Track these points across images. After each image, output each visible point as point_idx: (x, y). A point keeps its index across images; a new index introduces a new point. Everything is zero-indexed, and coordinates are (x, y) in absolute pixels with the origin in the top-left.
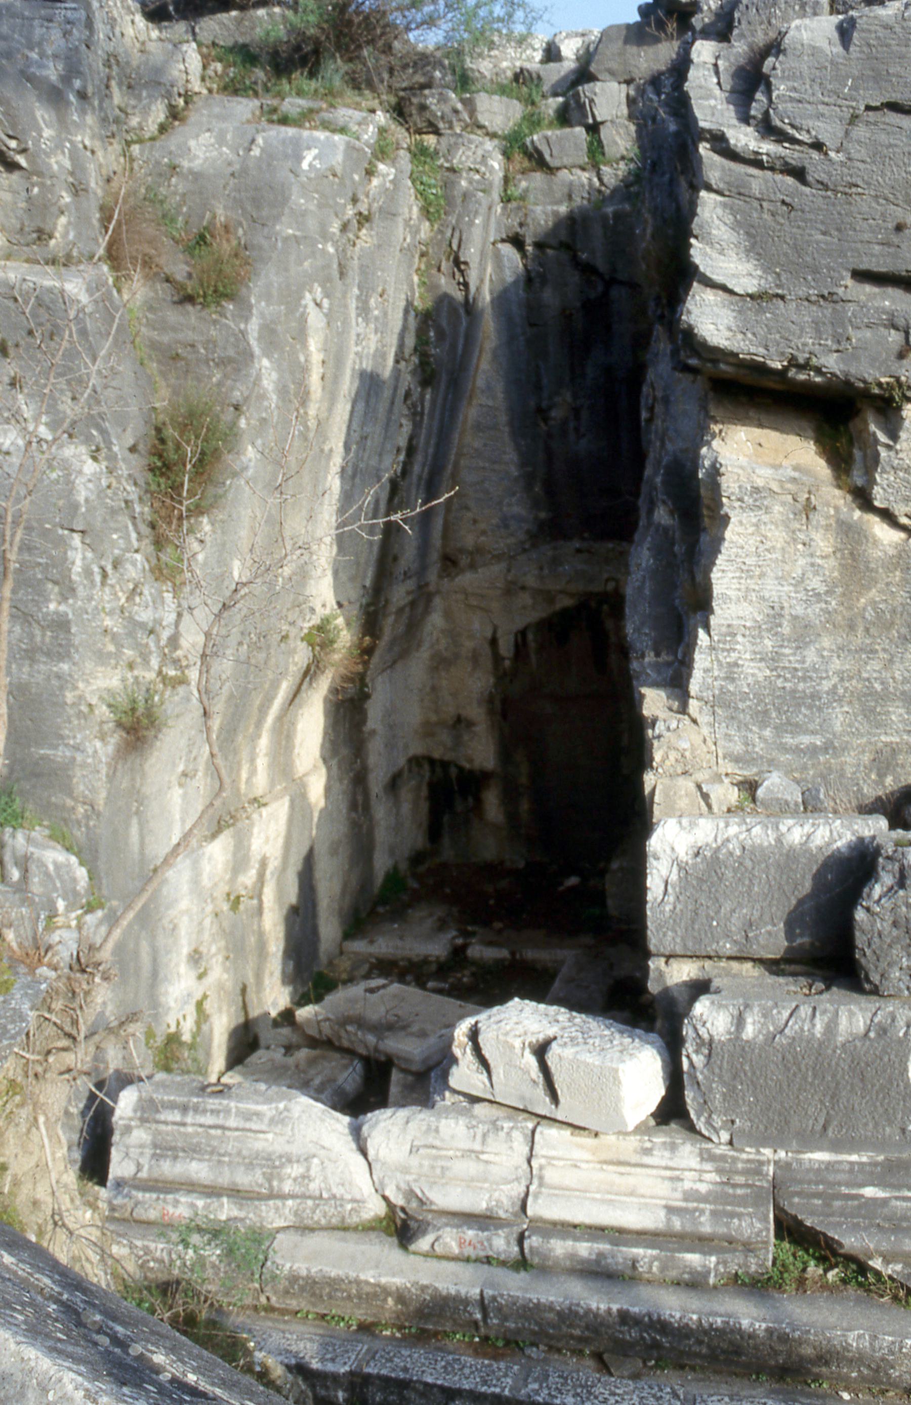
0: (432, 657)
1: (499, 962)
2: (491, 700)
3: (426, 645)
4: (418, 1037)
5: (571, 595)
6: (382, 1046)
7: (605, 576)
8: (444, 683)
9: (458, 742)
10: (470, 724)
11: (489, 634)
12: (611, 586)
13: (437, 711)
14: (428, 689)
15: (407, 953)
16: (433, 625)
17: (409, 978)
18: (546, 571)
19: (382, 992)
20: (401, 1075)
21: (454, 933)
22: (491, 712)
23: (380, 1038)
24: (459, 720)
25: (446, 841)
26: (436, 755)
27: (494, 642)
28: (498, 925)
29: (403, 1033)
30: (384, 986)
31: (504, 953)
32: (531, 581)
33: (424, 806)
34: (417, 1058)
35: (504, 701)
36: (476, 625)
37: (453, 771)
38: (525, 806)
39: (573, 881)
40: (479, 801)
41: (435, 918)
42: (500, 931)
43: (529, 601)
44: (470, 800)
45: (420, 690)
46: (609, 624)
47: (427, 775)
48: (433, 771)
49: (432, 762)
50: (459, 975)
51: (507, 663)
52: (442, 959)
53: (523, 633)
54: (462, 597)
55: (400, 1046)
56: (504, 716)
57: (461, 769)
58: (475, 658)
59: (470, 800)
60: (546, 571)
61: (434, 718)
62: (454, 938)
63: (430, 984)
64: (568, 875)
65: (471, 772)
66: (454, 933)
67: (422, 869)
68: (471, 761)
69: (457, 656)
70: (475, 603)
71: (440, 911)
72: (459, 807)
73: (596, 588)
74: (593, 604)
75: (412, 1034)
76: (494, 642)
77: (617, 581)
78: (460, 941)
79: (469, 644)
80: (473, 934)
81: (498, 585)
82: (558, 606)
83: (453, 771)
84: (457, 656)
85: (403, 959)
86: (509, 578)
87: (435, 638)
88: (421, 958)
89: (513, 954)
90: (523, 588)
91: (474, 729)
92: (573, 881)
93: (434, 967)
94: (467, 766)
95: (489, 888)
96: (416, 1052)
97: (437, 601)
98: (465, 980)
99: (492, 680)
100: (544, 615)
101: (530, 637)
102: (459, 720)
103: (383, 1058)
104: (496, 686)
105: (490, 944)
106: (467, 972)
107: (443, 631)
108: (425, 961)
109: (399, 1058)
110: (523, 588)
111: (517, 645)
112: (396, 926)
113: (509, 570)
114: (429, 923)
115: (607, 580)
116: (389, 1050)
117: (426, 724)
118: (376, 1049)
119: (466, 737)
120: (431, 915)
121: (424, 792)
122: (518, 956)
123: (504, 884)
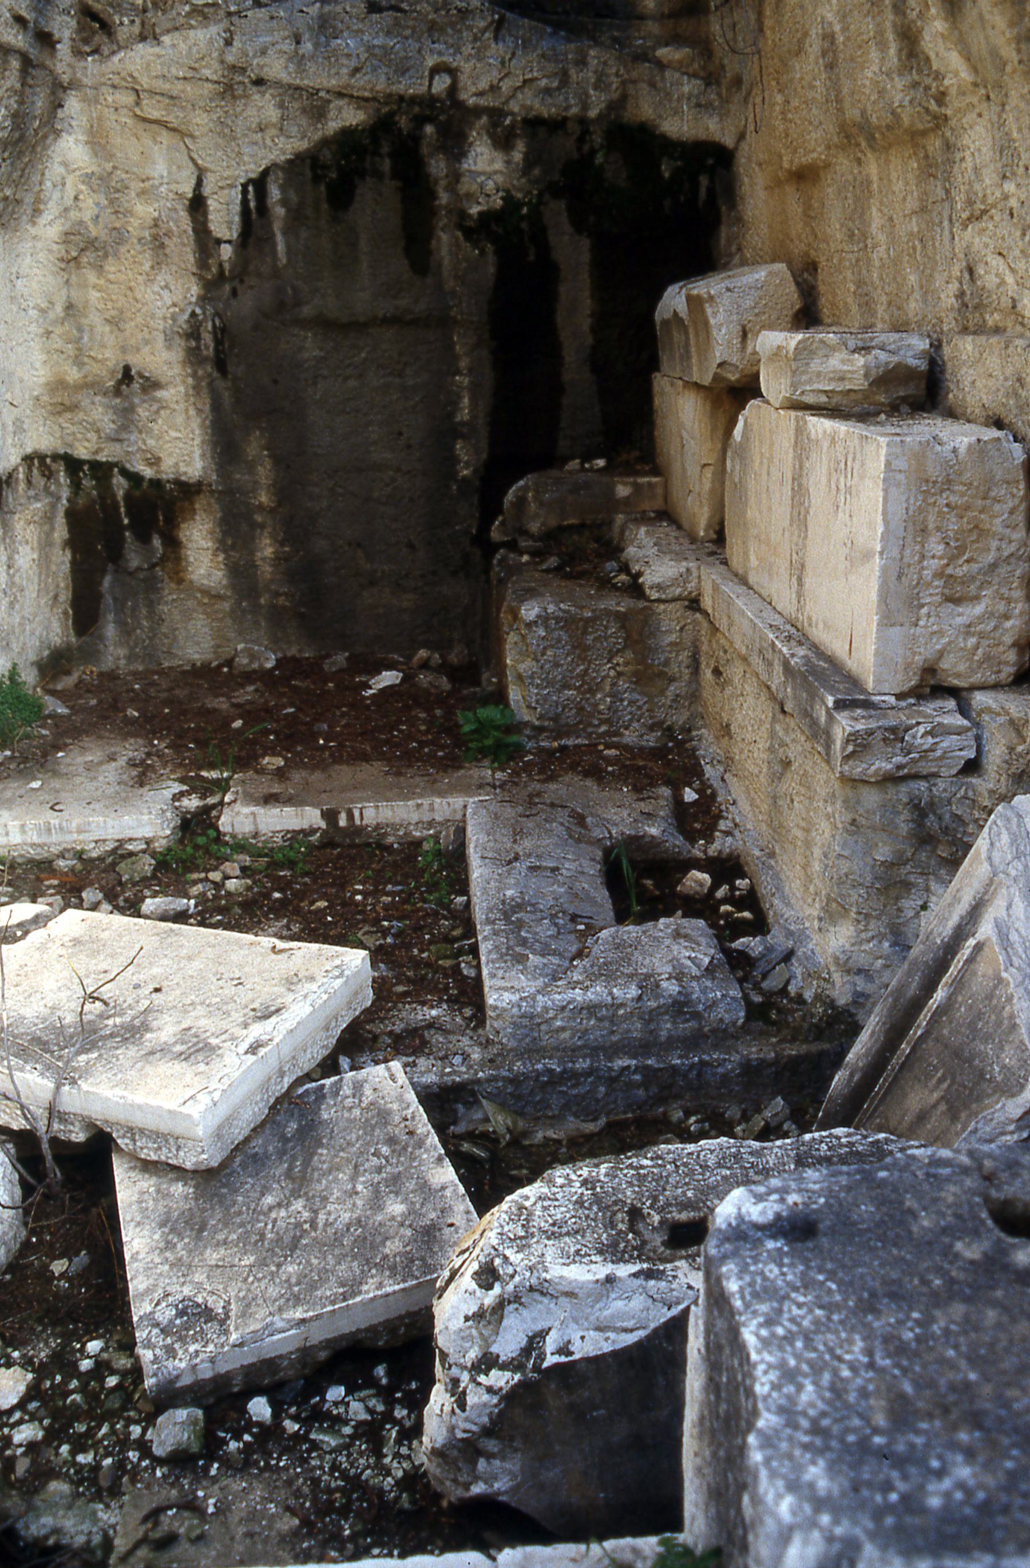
0: (67, 237)
1: (295, 836)
2: (193, 333)
3: (51, 212)
4: (185, 1057)
5: (360, 101)
6: (71, 1100)
7: (430, 62)
8: (94, 295)
9: (126, 417)
10: (151, 385)
11: (188, 190)
12: (441, 84)
13: (78, 361)
14: (59, 309)
15: (71, 839)
16: (65, 164)
17: (89, 895)
18: (308, 47)
19: (36, 936)
20: (148, 1183)
21: (177, 787)
22: (194, 357)
23: (66, 1077)
24: (127, 375)
25: (110, 631)
26: (82, 452)
27: (197, 204)
28: (273, 762)
29: (127, 1054)
30: (39, 921)
31: (311, 817)
32: (277, 68)
33: (62, 560)
34: (200, 1132)
35: (221, 335)
36: (160, 168)
37: (120, 484)
38: (266, 549)
39: (389, 678)
40: (173, 544)
41: (122, 761)
42: (280, 774)
43: (273, 114)
44: (157, 542)
45: (43, 311)
46: (437, 166)
47: (65, 493)
48: (76, 486)
49: (73, 465)
50: (215, 876)
51: (226, 252)
52: (159, 845)
53: (259, 184)
54: (129, 99)
55: (138, 1097)
56: (221, 364)
57: (134, 478)
58: (158, 243)
59: (157, 542)
60: (308, 47)
61: (73, 375)
62: (177, 797)
63: (150, 905)
64: (376, 669)
65: (156, 484)
66: (177, 787)
67: (66, 682)
68: (155, 461)
69: (119, 236)
70: (155, 114)
71: (132, 749)
72: (134, 560)
73: (412, 86)
74: (403, 122)
75: (162, 1051)
76: (197, 204)
77: (452, 72)
78: (192, 803)
79: (145, 211)
80: (222, 786)
81: (207, 73)
82: (333, 126)
83: (120, 484)
84: (119, 236)
85: (62, 855)
86: (230, 59)
87: (70, 192)
88: (110, 846)
89: (330, 816)
90: (259, 82)
91: (160, 394)
92: (389, 678)
93: (147, 865)
94: (148, 472)
95: (221, 704)
96: (194, 1110)
97: (73, 104)
98: (232, 884)
99: (195, 290)
100: (303, 145)
101: (275, 193)
102: (127, 375)
103: (79, 1136)
104: (203, 300)
105: (269, 799)
106: (232, 868)
107: (87, 178)
108: (120, 853)
109: (132, 1131)
110: (259, 82)
111: (245, 211)
112: (36, 784)
113: (229, 43)
114: (111, 772)
115: (435, 70)
116: (97, 1112)
117: (58, 385)
118: (53, 1111)
119: (143, 412)
120: (112, 758)
121: (61, 532)
122: (343, 822)
123: (247, 694)
